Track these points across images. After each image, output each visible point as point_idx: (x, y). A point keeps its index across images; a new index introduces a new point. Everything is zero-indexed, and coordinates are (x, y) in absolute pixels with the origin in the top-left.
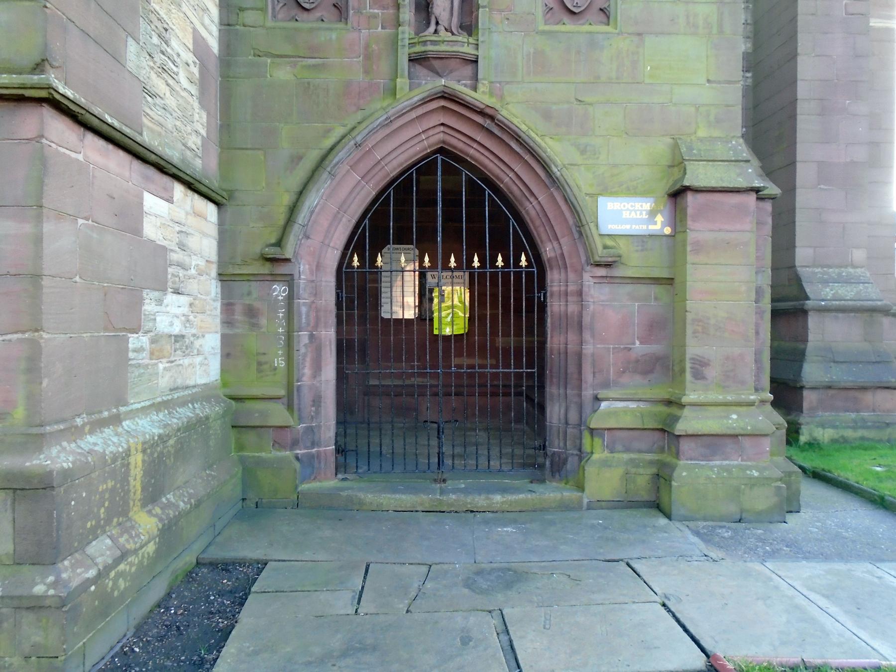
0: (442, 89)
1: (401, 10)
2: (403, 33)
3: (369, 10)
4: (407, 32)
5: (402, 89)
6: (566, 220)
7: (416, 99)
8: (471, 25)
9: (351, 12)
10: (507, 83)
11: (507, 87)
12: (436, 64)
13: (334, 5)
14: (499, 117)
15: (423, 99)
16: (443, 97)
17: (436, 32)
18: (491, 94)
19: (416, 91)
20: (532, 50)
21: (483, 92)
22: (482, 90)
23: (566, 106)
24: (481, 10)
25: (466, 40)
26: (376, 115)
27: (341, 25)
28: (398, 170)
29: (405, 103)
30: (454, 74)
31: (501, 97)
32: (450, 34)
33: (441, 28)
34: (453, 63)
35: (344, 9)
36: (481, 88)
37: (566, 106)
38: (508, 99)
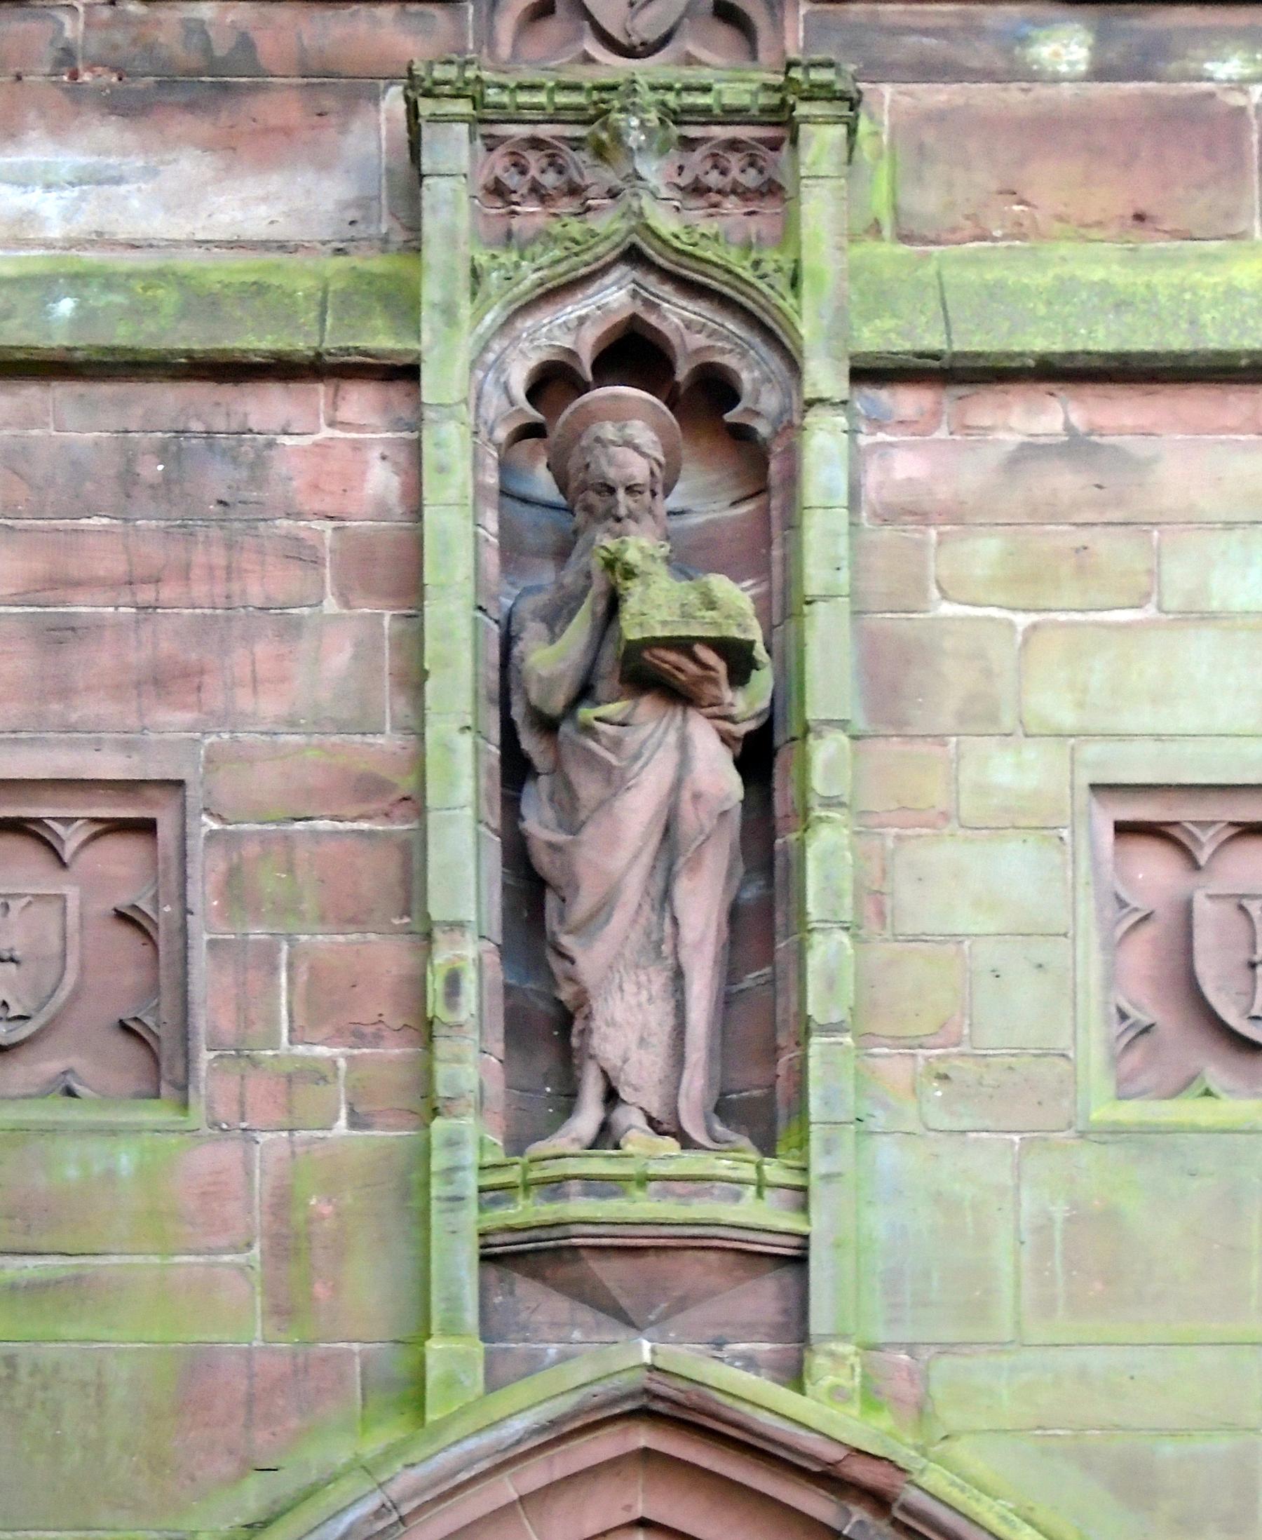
0: (642, 1379)
1: (442, 1047)
2: (453, 1143)
3: (287, 1049)
4: (469, 1141)
5: (451, 1382)
6: (532, 213)
7: (519, 1425)
8: (769, 1101)
9: (205, 1057)
10: (946, 1348)
11: (943, 1366)
12: (612, 1274)
13: (124, 1027)
14: (912, 1496)
15: (553, 1423)
16: (644, 1415)
17: (606, 1136)
18: (872, 1396)
19: (521, 1393)
20: (1059, 1211)
21: (837, 1393)
22: (829, 1380)
23: (1223, 1443)
24: (817, 1044)
25: (748, 1172)
26: (334, 1496)
27: (156, 1114)
28: (469, 1492)
29: (471, 1444)
30: (694, 1315)
31: (921, 1410)
32: (670, 1145)
33: (630, 1118)
34: (692, 1271)
35: (167, 1048)
36: (825, 1371)
37: (1223, 1443)
38: (951, 1417)
